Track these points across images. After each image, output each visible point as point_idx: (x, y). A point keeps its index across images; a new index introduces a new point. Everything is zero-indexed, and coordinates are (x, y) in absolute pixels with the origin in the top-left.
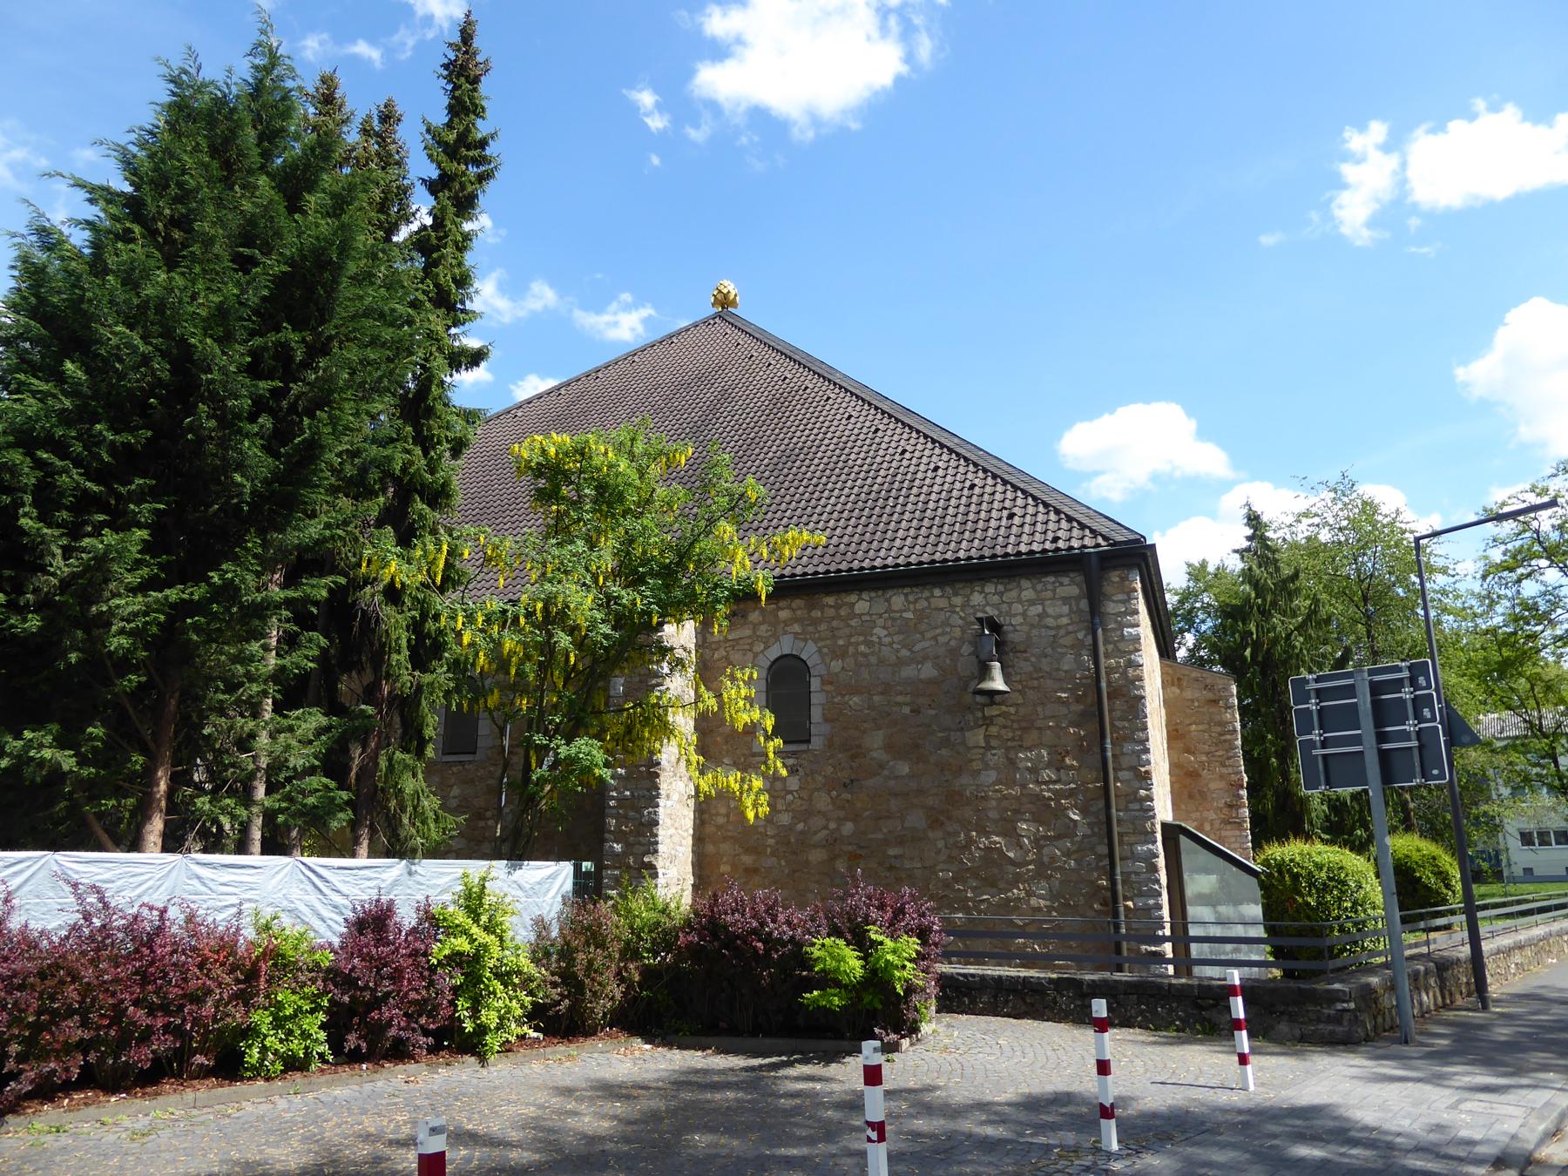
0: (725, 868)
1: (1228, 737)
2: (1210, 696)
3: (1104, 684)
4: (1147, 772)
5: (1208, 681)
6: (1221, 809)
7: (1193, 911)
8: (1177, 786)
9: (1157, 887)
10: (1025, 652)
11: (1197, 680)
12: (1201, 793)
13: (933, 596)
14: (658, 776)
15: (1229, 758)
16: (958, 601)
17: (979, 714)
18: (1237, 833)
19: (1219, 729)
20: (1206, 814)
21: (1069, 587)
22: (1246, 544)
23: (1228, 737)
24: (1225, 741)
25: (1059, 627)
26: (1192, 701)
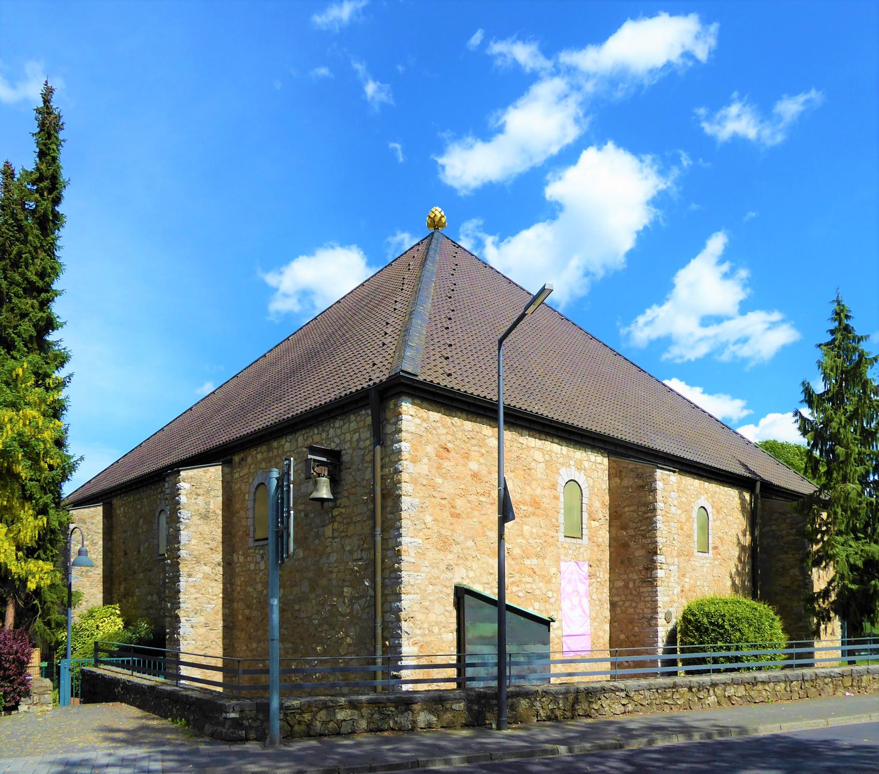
0: (240, 617)
1: (650, 515)
2: (640, 483)
3: (378, 489)
4: (399, 551)
5: (639, 471)
6: (640, 571)
7: (469, 648)
8: (614, 555)
9: (399, 632)
10: (350, 468)
11: (632, 470)
12: (629, 559)
13: (314, 434)
14: (179, 564)
15: (649, 531)
16: (324, 435)
17: (330, 515)
18: (650, 589)
19: (644, 509)
20: (631, 575)
21: (365, 417)
22: (829, 338)
23: (650, 515)
24: (647, 518)
25: (365, 448)
26: (628, 488)
